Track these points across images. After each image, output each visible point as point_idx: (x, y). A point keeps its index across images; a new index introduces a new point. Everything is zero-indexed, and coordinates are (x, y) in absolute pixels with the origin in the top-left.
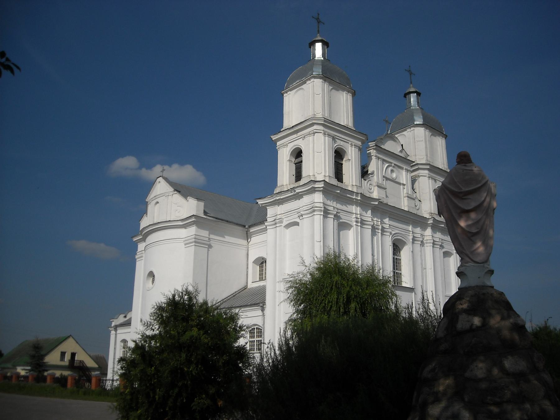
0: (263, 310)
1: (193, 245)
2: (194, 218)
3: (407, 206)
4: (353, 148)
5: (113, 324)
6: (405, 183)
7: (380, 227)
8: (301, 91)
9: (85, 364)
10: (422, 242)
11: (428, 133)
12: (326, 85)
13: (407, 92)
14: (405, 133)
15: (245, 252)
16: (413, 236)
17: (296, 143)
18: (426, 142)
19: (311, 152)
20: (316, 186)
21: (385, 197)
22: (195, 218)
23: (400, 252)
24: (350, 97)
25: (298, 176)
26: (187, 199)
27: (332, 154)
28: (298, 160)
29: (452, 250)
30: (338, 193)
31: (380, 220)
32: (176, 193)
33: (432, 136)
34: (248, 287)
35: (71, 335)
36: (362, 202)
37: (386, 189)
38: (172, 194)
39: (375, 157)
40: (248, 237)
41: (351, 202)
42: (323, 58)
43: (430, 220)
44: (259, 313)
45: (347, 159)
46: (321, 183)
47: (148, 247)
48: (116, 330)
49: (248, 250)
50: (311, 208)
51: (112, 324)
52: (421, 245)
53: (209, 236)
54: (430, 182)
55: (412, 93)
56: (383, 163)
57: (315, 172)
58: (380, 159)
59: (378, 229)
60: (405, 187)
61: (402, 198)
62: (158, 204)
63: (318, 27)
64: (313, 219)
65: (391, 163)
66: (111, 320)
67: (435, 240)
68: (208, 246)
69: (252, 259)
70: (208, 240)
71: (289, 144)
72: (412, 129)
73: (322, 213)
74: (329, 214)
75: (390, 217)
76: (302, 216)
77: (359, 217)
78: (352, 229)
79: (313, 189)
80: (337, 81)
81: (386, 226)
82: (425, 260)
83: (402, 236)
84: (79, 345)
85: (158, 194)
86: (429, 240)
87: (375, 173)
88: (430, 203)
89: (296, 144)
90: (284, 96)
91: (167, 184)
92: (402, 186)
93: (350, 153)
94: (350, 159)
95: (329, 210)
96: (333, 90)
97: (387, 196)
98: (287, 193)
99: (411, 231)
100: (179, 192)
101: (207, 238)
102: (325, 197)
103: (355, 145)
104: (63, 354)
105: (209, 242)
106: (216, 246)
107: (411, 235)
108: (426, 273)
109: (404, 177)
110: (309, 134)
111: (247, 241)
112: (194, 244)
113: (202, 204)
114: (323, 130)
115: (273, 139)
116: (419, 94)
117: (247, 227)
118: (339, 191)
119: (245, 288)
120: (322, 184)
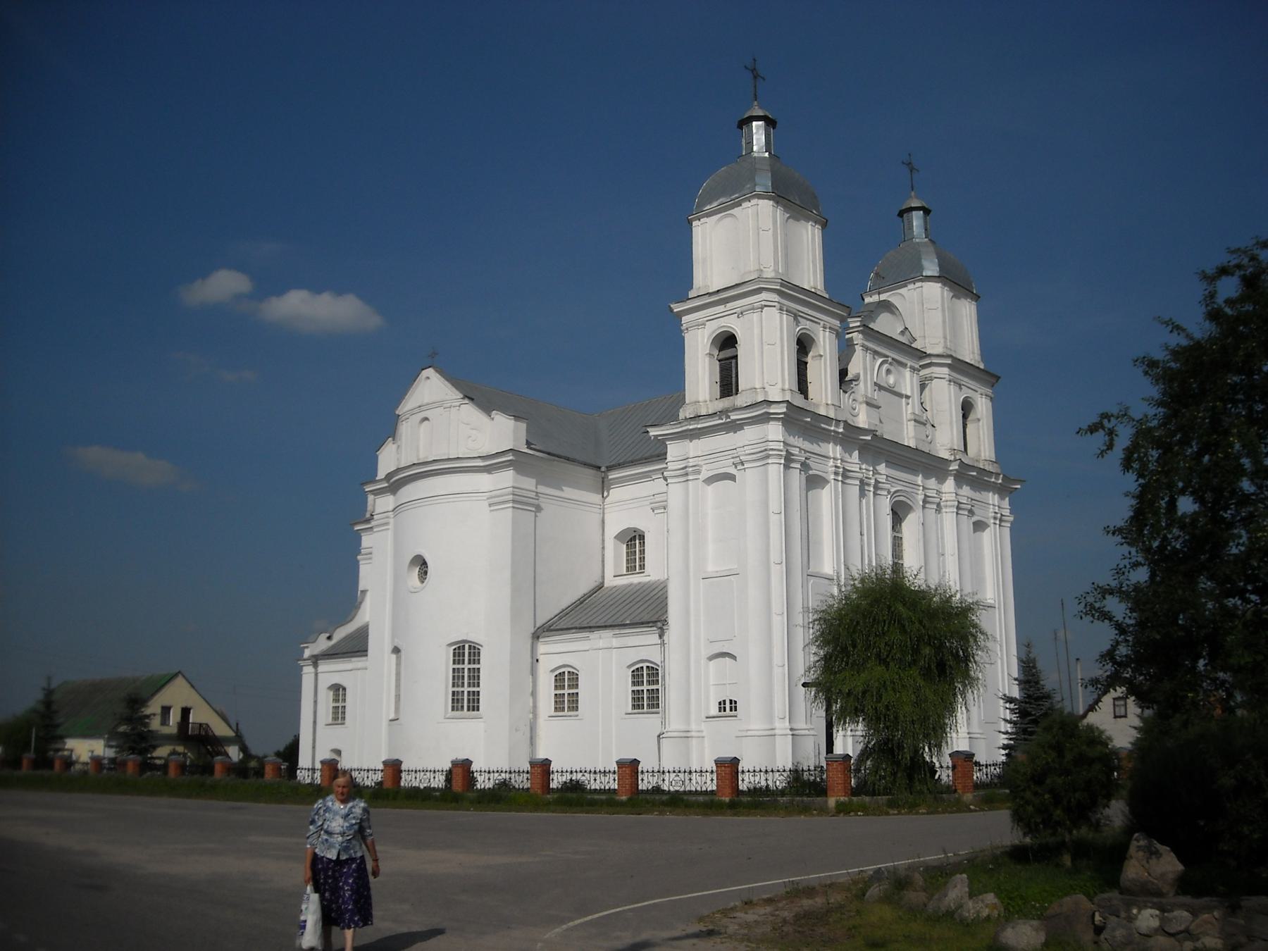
1: (509, 507)
2: (511, 454)
3: (913, 438)
4: (827, 333)
5: (307, 653)
6: (909, 394)
7: (873, 481)
8: (728, 220)
9: (212, 731)
10: (938, 505)
11: (947, 293)
12: (779, 211)
13: (904, 208)
14: (903, 291)
15: (598, 518)
16: (925, 495)
18: (943, 311)
19: (756, 342)
20: (772, 411)
21: (878, 423)
22: (513, 455)
23: (900, 525)
24: (817, 231)
25: (728, 385)
26: (490, 416)
27: (795, 347)
28: (728, 353)
29: (988, 518)
30: (807, 422)
31: (871, 469)
33: (954, 299)
34: (606, 585)
35: (179, 672)
36: (846, 436)
37: (880, 407)
38: (458, 404)
39: (861, 348)
40: (603, 487)
41: (826, 436)
42: (767, 153)
43: (953, 464)
44: (655, 638)
45: (817, 354)
46: (781, 405)
47: (407, 508)
48: (315, 665)
49: (604, 513)
51: (304, 652)
52: (936, 510)
53: (536, 488)
54: (952, 390)
55: (914, 210)
56: (874, 358)
57: (765, 381)
58: (870, 350)
59: (869, 485)
60: (910, 401)
61: (905, 423)
62: (426, 422)
63: (755, 87)
65: (887, 357)
66: (302, 646)
67: (960, 501)
68: (536, 508)
69: (613, 529)
70: (535, 497)
71: (707, 323)
72: (918, 284)
73: (783, 461)
74: (793, 461)
75: (888, 461)
76: (742, 463)
77: (839, 465)
78: (828, 487)
79: (766, 416)
80: (798, 202)
81: (882, 479)
82: (943, 538)
83: (907, 496)
84: (196, 690)
85: (426, 401)
86: (950, 501)
87: (862, 377)
91: (446, 382)
92: (904, 399)
93: (822, 343)
94: (822, 354)
95: (793, 455)
96: (791, 220)
97: (881, 422)
98: (711, 419)
99: (921, 484)
100: (471, 399)
101: (533, 491)
102: (786, 431)
103: (830, 328)
104: (166, 710)
105: (538, 499)
106: (549, 508)
107: (920, 492)
108: (944, 562)
109: (907, 381)
111: (601, 496)
112: (511, 505)
114: (778, 302)
115: (675, 310)
116: (927, 212)
117: (603, 469)
118: (809, 420)
119: (601, 586)
120: (783, 407)
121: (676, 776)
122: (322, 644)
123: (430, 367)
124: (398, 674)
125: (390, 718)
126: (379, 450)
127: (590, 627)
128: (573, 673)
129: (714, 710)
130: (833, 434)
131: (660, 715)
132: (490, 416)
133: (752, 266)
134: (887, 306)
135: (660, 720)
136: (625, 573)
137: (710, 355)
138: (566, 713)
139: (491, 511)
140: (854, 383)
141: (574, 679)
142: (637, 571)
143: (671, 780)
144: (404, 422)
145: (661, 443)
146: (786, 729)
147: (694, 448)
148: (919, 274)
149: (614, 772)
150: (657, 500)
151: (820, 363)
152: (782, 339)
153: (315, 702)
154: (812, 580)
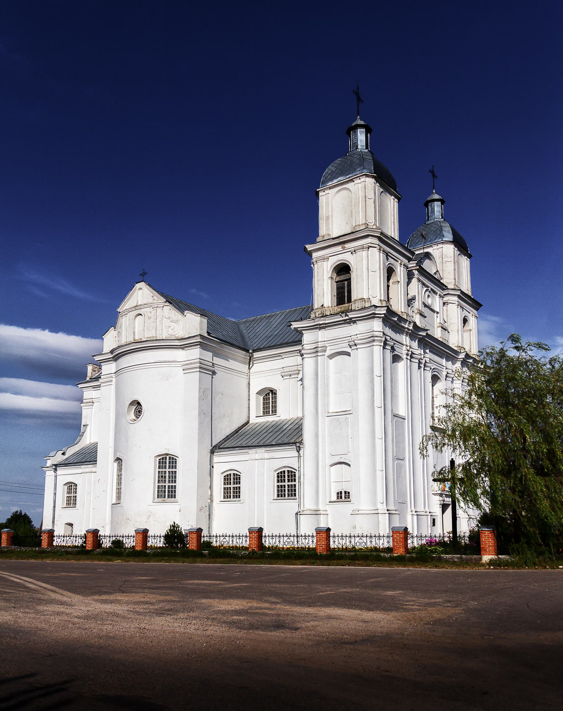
0: (299, 450)
4: (402, 268)
5: (49, 463)
8: (345, 192)
15: (245, 382)
17: (341, 257)
20: (377, 312)
26: (184, 314)
32: (169, 305)
40: (250, 362)
50: (370, 337)
57: (370, 295)
58: (421, 282)
62: (140, 316)
64: (372, 351)
69: (255, 389)
72: (440, 246)
88: (458, 335)
89: (340, 259)
90: (320, 195)
94: (399, 281)
110: (362, 248)
113: (205, 321)
114: (378, 245)
115: (308, 250)
117: (251, 351)
119: (248, 422)
120: (384, 310)
121: (288, 539)
122: (59, 458)
123: (142, 281)
124: (119, 476)
125: (113, 503)
126: (104, 335)
127: (249, 446)
128: (237, 474)
129: (334, 498)
130: (406, 330)
131: (297, 501)
132: (184, 314)
133: (361, 221)
134: (428, 256)
135: (298, 503)
136: (262, 415)
137: (332, 278)
138: (232, 499)
139: (184, 373)
140: (413, 301)
141: (237, 478)
142: (270, 414)
143: (284, 541)
144: (124, 317)
145: (299, 333)
146: (385, 510)
147: (322, 335)
148: (440, 240)
149: (246, 536)
150: (285, 370)
151: (398, 286)
152: (380, 268)
153: (55, 494)
154: (396, 419)
